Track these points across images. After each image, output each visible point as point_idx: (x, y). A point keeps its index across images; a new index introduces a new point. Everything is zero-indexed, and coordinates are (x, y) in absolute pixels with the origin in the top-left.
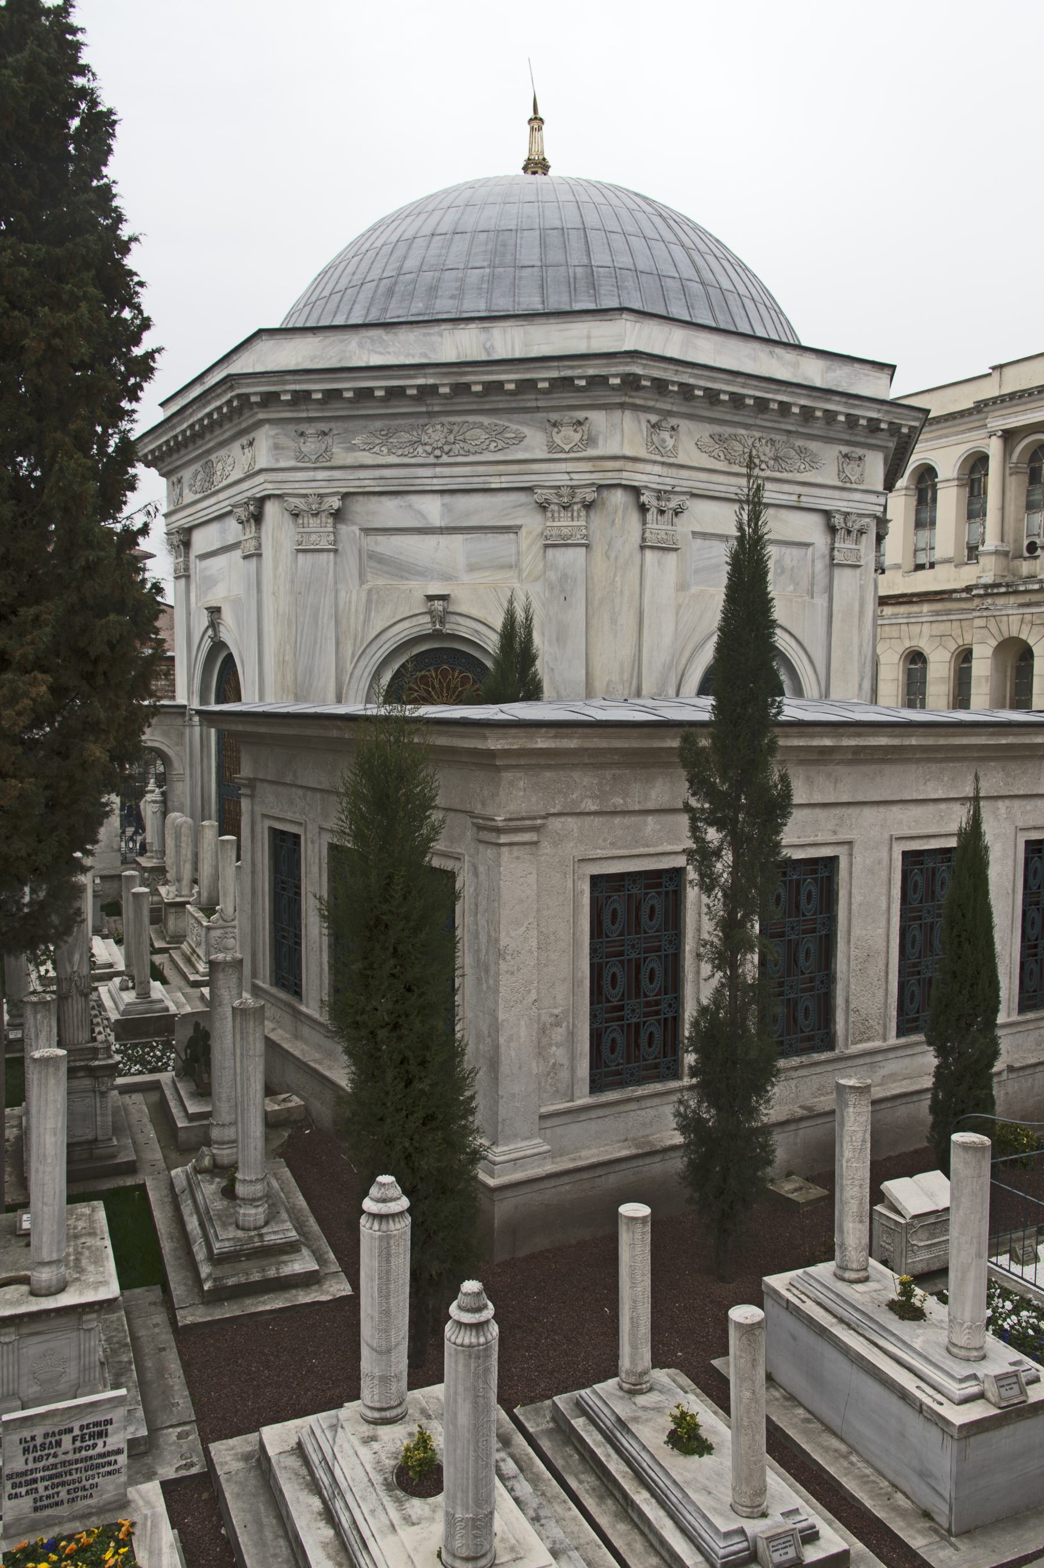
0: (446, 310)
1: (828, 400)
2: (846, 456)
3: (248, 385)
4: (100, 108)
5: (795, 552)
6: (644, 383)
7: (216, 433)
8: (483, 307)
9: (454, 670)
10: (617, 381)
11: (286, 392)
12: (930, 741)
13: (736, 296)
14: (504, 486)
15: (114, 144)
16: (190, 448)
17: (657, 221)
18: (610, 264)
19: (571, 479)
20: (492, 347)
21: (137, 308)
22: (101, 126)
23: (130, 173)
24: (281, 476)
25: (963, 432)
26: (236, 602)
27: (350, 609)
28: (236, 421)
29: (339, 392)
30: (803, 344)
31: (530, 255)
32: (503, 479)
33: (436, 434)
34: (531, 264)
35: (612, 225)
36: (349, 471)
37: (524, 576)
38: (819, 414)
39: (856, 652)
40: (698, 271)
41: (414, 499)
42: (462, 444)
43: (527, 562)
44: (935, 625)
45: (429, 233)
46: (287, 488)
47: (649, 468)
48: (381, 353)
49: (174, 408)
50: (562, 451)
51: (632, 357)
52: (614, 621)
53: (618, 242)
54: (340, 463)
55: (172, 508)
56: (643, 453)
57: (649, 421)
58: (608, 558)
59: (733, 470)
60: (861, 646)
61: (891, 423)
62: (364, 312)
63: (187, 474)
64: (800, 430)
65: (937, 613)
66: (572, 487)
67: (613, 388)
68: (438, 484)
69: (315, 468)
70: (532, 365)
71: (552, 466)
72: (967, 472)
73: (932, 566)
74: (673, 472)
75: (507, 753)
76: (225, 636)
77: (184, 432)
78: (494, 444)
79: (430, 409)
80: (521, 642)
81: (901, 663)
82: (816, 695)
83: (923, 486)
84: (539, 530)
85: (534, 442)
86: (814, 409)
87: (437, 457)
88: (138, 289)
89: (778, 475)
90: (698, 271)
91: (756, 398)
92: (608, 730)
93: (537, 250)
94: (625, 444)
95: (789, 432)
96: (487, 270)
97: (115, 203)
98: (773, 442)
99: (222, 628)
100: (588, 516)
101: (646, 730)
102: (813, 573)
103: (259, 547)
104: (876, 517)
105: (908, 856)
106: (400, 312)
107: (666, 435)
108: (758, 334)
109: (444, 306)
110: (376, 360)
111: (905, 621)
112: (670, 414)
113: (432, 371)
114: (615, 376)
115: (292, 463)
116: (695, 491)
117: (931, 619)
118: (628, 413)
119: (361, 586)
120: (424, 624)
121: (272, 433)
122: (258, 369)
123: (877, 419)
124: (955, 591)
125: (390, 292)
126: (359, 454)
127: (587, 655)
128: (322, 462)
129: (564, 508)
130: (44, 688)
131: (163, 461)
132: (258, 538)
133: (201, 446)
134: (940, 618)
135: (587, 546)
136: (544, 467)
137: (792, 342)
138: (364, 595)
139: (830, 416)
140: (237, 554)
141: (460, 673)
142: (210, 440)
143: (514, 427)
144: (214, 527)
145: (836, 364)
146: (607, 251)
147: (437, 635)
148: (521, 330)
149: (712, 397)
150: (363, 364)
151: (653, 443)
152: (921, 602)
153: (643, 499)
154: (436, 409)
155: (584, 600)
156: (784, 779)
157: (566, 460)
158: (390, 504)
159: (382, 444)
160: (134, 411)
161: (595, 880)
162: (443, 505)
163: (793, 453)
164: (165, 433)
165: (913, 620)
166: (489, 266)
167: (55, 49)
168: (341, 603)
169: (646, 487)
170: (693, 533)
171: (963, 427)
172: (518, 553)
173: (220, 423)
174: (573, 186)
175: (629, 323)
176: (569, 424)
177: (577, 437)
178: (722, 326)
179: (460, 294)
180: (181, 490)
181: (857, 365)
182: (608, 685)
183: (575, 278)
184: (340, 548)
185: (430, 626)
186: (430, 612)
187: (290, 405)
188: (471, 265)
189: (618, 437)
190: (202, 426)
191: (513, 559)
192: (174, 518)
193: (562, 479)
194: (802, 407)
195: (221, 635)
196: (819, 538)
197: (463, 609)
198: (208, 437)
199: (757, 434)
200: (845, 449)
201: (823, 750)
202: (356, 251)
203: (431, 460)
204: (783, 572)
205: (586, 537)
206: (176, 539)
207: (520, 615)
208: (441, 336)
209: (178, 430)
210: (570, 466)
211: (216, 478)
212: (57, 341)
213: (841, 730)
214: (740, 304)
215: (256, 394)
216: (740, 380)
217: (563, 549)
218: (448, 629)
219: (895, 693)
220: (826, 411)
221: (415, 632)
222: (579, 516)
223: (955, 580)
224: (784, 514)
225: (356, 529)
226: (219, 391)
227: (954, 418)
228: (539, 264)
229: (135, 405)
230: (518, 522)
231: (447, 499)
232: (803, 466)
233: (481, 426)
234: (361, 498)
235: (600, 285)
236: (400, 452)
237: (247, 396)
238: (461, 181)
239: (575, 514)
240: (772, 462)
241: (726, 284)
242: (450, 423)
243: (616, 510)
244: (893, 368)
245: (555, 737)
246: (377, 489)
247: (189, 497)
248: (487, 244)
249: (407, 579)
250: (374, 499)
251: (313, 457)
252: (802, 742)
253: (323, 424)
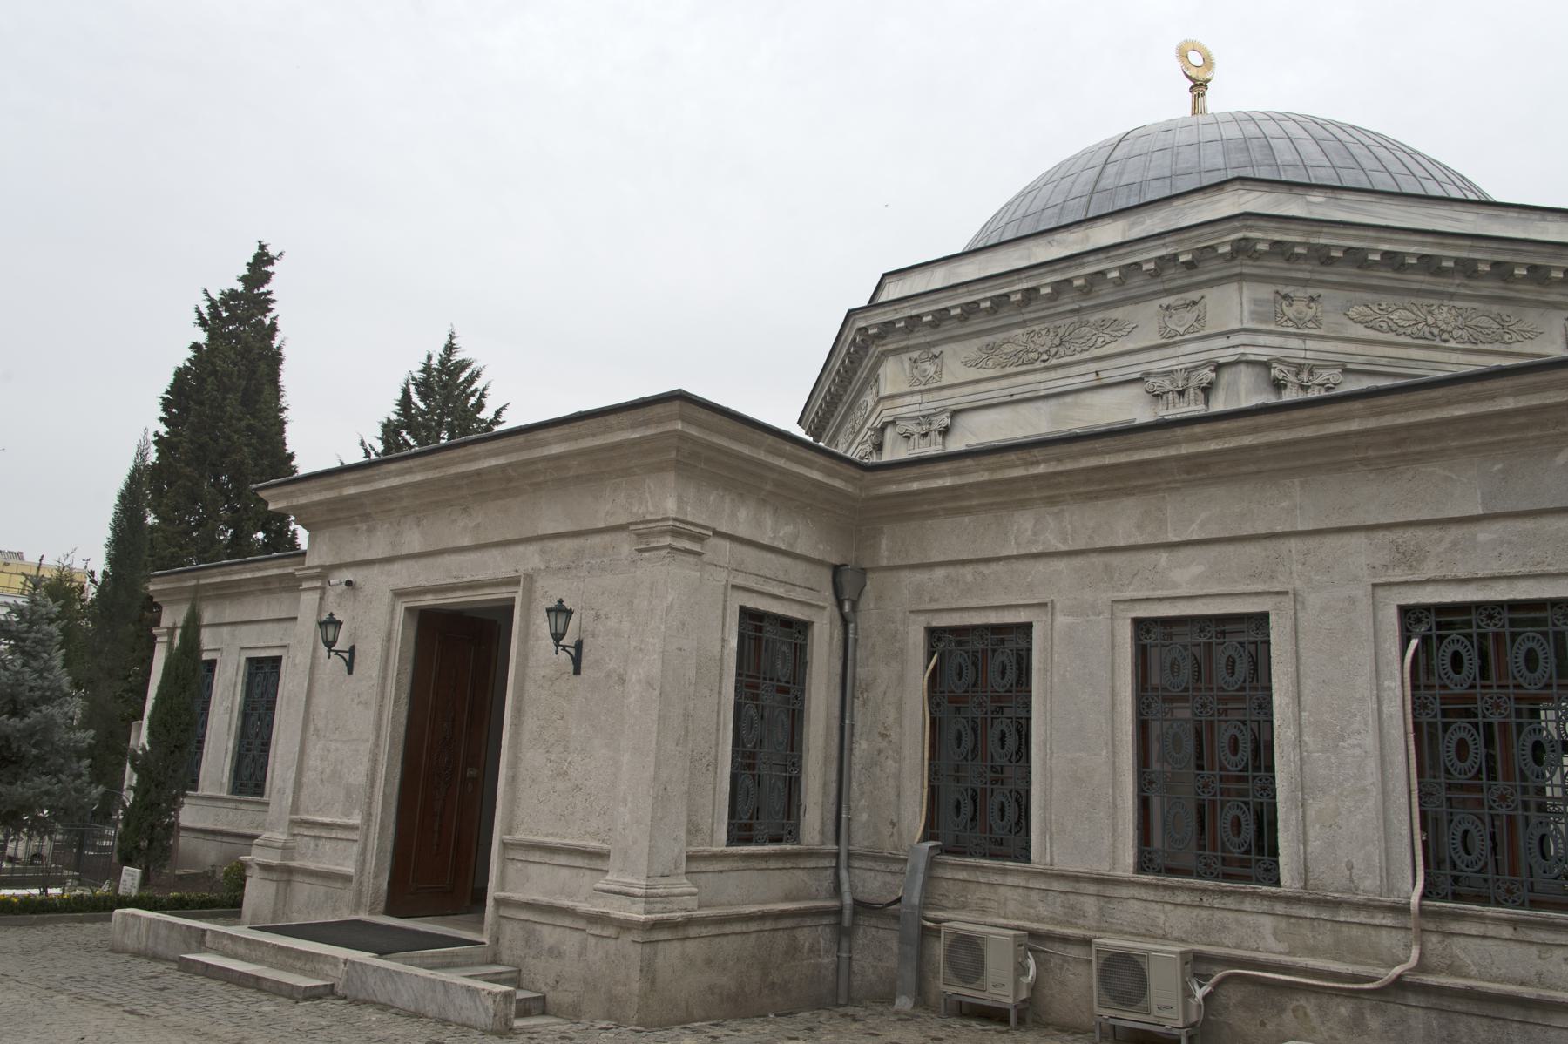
1: (1082, 265)
2: (1168, 308)
15: (109, 534)
23: (287, 378)
47: (908, 400)
74: (935, 395)
105: (250, 660)
112: (930, 345)
161: (1138, 623)
216: (960, 291)
224: (1087, 398)
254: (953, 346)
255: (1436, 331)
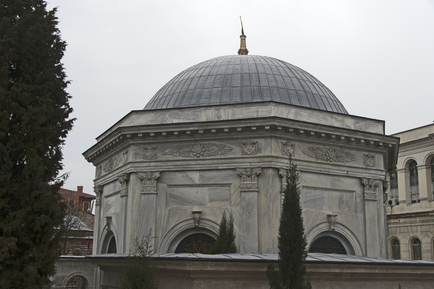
0: (204, 102)
1: (356, 134)
2: (366, 156)
3: (126, 131)
4: (61, 41)
5: (348, 194)
6: (279, 128)
7: (115, 149)
8: (218, 101)
9: (203, 243)
10: (268, 128)
11: (140, 133)
12: (385, 271)
13: (319, 96)
14: (224, 168)
16: (105, 155)
17: (287, 70)
18: (267, 85)
19: (251, 165)
20: (220, 116)
21: (68, 105)
22: (61, 46)
23: (66, 61)
24: (137, 165)
25: (426, 147)
26: (117, 215)
27: (161, 217)
28: (122, 144)
29: (161, 133)
30: (350, 114)
31: (237, 82)
32: (224, 165)
33: (198, 148)
34: (237, 86)
35: (269, 71)
36: (163, 163)
37: (232, 203)
38: (353, 139)
39: (377, 237)
40: (303, 87)
41: (189, 173)
42: (208, 152)
43: (233, 198)
44: (422, 227)
45: (199, 76)
46: (139, 170)
47: (283, 161)
48: (177, 119)
49: (100, 139)
50: (247, 154)
51: (274, 119)
52: (269, 223)
53: (271, 77)
54: (160, 159)
55: (97, 177)
56: (280, 155)
57: (282, 143)
58: (267, 196)
59: (318, 162)
60: (380, 234)
61: (384, 143)
62: (173, 104)
63: (103, 165)
64: (346, 146)
65: (423, 222)
66: (251, 168)
67: (267, 130)
68: (198, 167)
69: (150, 162)
70: (235, 122)
71: (243, 160)
72: (429, 162)
73: (419, 201)
75: (195, 272)
76: (113, 229)
77: (103, 148)
78: (220, 152)
79: (196, 139)
80: (228, 231)
81: (410, 244)
82: (361, 255)
83: (412, 168)
84: (239, 185)
85: (236, 151)
86: (351, 138)
87: (198, 157)
88: (69, 99)
89: (338, 163)
90: (303, 87)
91: (326, 134)
92: (239, 263)
93: (239, 81)
94: (273, 152)
95: (341, 147)
96: (220, 88)
97: (63, 71)
98: (335, 150)
99: (111, 226)
100: (258, 180)
101: (255, 264)
102: (356, 203)
103: (127, 192)
104: (383, 181)
106: (187, 104)
107: (289, 148)
108: (329, 110)
109: (204, 101)
110: (175, 121)
111: (410, 225)
112: (291, 140)
113: (196, 125)
114: (267, 126)
115: (142, 160)
116: (302, 170)
117: (421, 224)
118: (273, 140)
119: (166, 208)
120: (191, 224)
121: (135, 148)
122: (131, 125)
123: (378, 142)
124: (429, 212)
125: (184, 97)
126: (169, 156)
127: (258, 237)
128: (154, 159)
129: (248, 176)
130: (14, 243)
131: (95, 160)
132: (127, 189)
133: (109, 154)
134: (424, 224)
135: (258, 192)
136: (240, 160)
137: (343, 113)
138: (167, 211)
139: (358, 141)
140: (119, 195)
141: (206, 244)
142: (112, 152)
143: (228, 145)
144: (111, 185)
145: (359, 121)
146: (267, 80)
147: (196, 228)
148: (231, 109)
149: (307, 133)
150: (171, 123)
151: (284, 151)
152: (416, 217)
153: (280, 173)
154: (198, 139)
155: (257, 214)
156: (309, 284)
157: (249, 158)
158: (179, 175)
159: (177, 152)
160: (64, 141)
162: (200, 175)
163: (344, 155)
164: (96, 149)
165: (413, 225)
166: (221, 87)
167: (47, 22)
168: (158, 215)
169: (282, 168)
170: (303, 186)
171: (423, 145)
172: (230, 194)
173: (116, 145)
174: (254, 58)
175: (273, 107)
176: (250, 144)
177: (253, 149)
178: (313, 107)
179: (210, 97)
180: (101, 171)
181: (368, 121)
182: (267, 250)
183: (254, 90)
184: (159, 193)
185: (193, 224)
186: (194, 219)
187: (142, 138)
188: (214, 87)
189: (270, 149)
190: (109, 146)
191: (228, 197)
192: (97, 182)
193: (248, 165)
194: (346, 137)
195: (111, 228)
196: (358, 189)
197: (208, 217)
198: (111, 150)
199: (328, 148)
200: (366, 153)
201: (336, 274)
202: (172, 82)
203: (196, 158)
204: (343, 203)
205: (257, 188)
206: (97, 189)
207: (228, 219)
208: (201, 112)
209: (101, 148)
210: (250, 160)
211: (113, 166)
212: (34, 117)
213: (342, 266)
214: (320, 99)
215: (129, 134)
217: (248, 193)
218: (201, 225)
219: (408, 257)
220: (356, 138)
221: (187, 227)
222: (254, 180)
223: (429, 207)
224: (342, 179)
225: (165, 185)
226: (116, 133)
227: (422, 141)
228: (240, 86)
229: (64, 139)
230: (230, 182)
231: (202, 173)
232: (348, 160)
233: (215, 145)
234: (168, 173)
235: (263, 93)
236: (184, 155)
237: (126, 135)
238: (213, 58)
239: (253, 179)
240: (335, 158)
241: (314, 92)
242: (203, 144)
243: (270, 177)
244: (384, 122)
245: (215, 265)
246: (174, 169)
247: (103, 173)
248: (221, 79)
249: (185, 205)
250: (173, 173)
251: (150, 158)
252: (325, 271)
253: (154, 145)
254: (298, 143)
255: (328, 158)
